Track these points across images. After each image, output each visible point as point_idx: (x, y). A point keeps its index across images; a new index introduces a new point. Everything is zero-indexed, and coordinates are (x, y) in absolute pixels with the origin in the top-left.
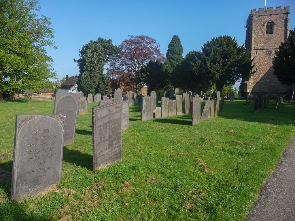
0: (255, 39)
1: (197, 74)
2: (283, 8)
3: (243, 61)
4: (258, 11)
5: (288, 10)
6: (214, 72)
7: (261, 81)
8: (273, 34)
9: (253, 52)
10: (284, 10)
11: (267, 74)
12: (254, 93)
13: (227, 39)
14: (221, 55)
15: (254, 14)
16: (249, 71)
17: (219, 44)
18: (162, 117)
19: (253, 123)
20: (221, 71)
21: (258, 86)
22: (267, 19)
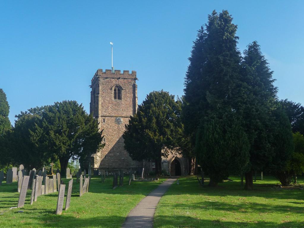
0: (102, 103)
1: (37, 145)
2: (130, 73)
3: (91, 132)
4: (105, 72)
5: (136, 76)
6: (59, 145)
7: (110, 154)
8: (121, 100)
9: (100, 119)
10: (131, 75)
11: (116, 146)
12: (102, 168)
13: (73, 105)
14: (67, 123)
15: (100, 75)
16: (98, 144)
17: (65, 111)
18: (45, 193)
19: (116, 195)
20: (68, 144)
21: (107, 159)
22: (115, 82)
